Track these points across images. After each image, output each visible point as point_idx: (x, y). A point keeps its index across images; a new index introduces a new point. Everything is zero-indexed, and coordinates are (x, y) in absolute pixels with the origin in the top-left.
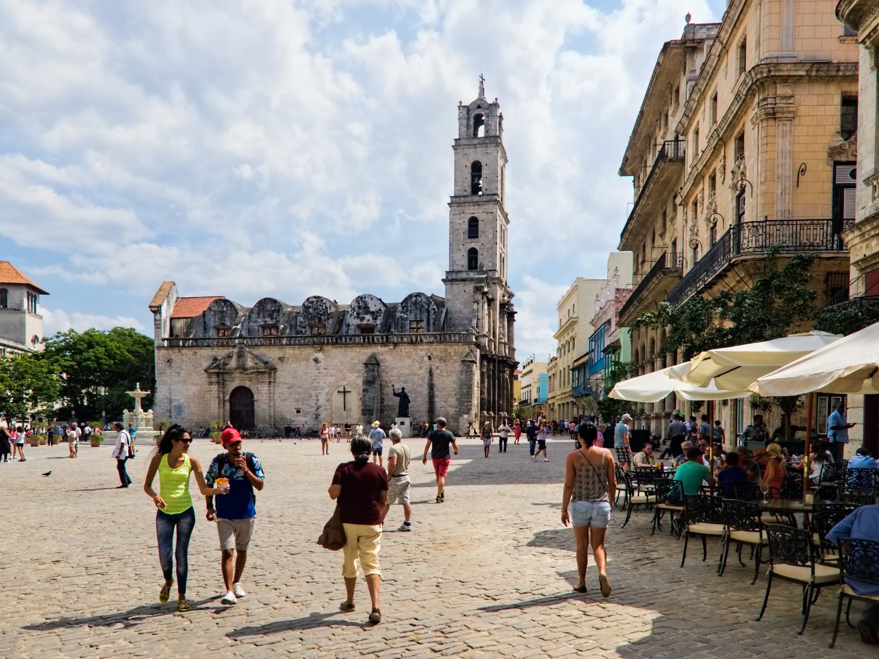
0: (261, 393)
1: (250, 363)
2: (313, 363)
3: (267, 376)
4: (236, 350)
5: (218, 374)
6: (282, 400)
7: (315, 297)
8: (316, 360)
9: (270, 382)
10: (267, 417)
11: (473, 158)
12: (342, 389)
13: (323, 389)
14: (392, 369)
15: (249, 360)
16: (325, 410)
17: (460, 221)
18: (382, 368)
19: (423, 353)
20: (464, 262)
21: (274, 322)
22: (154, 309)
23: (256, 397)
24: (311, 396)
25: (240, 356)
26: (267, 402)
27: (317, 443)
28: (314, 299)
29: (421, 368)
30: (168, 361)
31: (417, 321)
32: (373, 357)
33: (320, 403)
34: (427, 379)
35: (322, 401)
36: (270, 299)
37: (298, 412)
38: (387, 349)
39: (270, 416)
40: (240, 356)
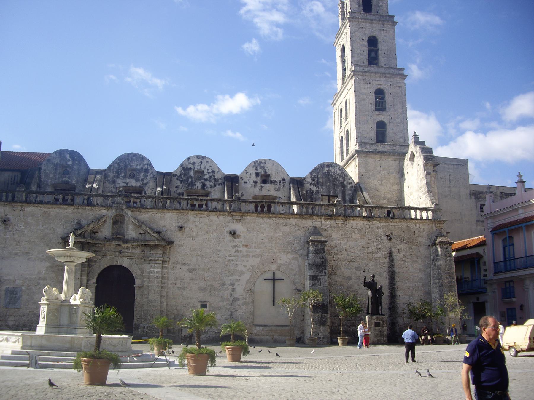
0: (148, 275)
1: (131, 232)
2: (229, 237)
3: (160, 252)
6: (179, 289)
7: (198, 157)
8: (233, 233)
9: (163, 262)
11: (369, 33)
12: (269, 276)
13: (242, 273)
14: (341, 251)
15: (131, 227)
16: (245, 304)
17: (366, 91)
19: (381, 231)
20: (372, 135)
21: (138, 184)
23: (138, 282)
24: (224, 284)
26: (159, 289)
28: (195, 160)
29: (379, 250)
31: (329, 196)
33: (236, 295)
34: (386, 265)
35: (240, 290)
38: (333, 222)
40: (118, 221)
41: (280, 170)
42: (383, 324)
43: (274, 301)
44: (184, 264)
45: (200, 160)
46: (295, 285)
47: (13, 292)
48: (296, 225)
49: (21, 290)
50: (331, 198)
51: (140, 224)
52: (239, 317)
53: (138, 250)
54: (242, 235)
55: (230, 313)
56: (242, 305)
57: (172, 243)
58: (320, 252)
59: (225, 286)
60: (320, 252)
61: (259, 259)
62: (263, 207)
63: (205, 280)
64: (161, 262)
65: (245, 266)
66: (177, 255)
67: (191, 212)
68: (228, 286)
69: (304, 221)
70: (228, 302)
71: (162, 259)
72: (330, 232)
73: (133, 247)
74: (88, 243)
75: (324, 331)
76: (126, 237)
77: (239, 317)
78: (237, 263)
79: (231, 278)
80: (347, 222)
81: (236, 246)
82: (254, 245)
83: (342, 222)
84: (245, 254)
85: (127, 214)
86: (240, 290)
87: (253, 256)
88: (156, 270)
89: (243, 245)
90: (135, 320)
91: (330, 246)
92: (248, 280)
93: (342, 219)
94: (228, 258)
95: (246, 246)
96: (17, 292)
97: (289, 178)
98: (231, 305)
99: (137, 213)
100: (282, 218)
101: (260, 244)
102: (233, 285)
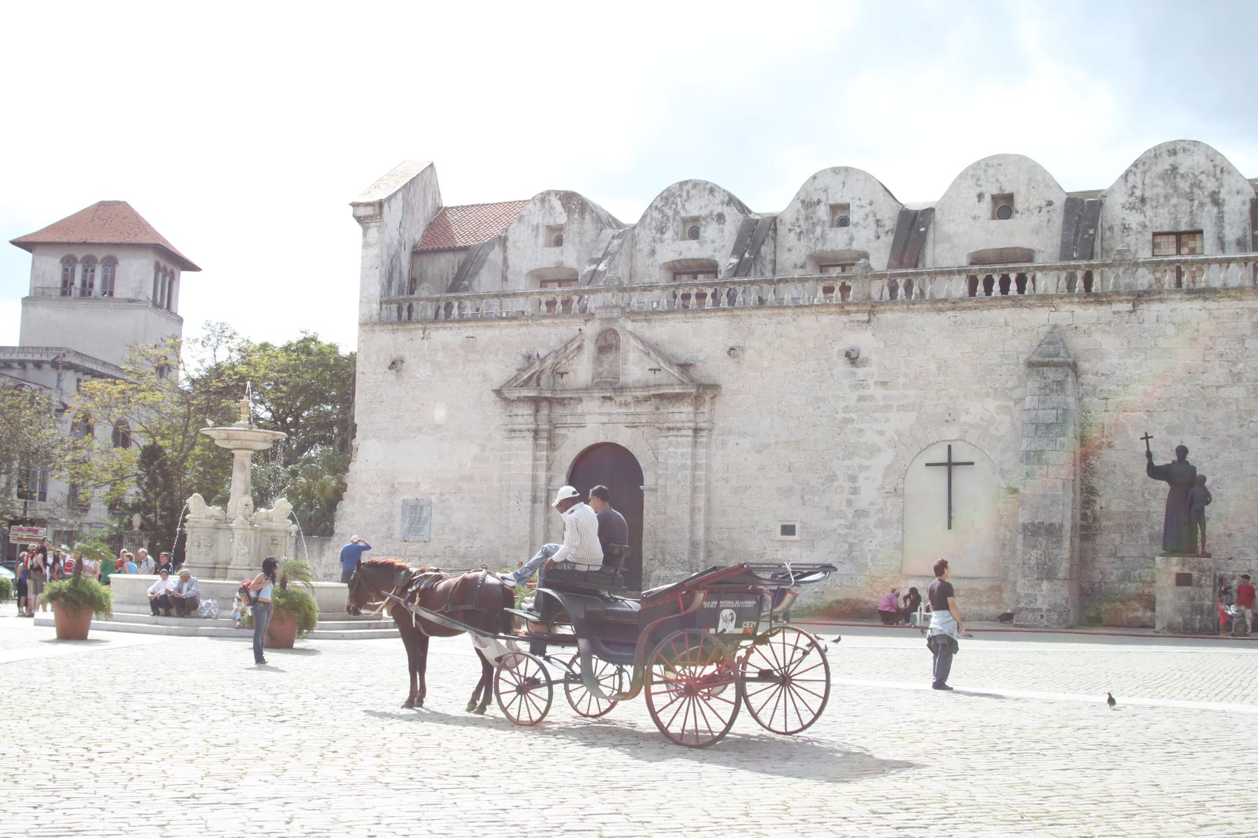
2: (842, 366)
4: (592, 329)
5: (536, 401)
7: (835, 171)
8: (852, 358)
10: (685, 547)
13: (873, 451)
16: (881, 524)
18: (1089, 379)
22: (362, 212)
24: (832, 478)
25: (607, 345)
27: (911, 651)
30: (393, 365)
32: (1055, 337)
33: (862, 502)
35: (869, 494)
36: (696, 184)
37: (788, 530)
39: (694, 544)
40: (607, 345)
41: (1040, 178)
42: (1200, 579)
43: (950, 517)
44: (744, 435)
45: (841, 176)
46: (1003, 477)
47: (415, 507)
48: (1006, 324)
49: (430, 504)
50: (1184, 239)
51: (651, 348)
52: (869, 556)
53: (647, 408)
54: (874, 358)
55: (846, 546)
56: (876, 527)
57: (715, 387)
58: (1052, 391)
59: (836, 483)
60: (1052, 391)
61: (915, 414)
62: (988, 283)
63: (790, 470)
64: (690, 432)
65: (881, 433)
66: (728, 413)
67: (755, 312)
68: (842, 482)
69: (1026, 313)
70: (842, 521)
71: (691, 425)
72: (1097, 337)
73: (638, 401)
74: (546, 399)
75: (1048, 595)
76: (622, 379)
77: (869, 556)
78: (863, 426)
79: (848, 462)
80: (1145, 306)
81: (861, 384)
82: (902, 380)
83: (1129, 306)
84: (881, 403)
85: (623, 328)
86: (869, 494)
87: (902, 408)
88: (679, 451)
89: (876, 383)
90: (644, 564)
91: (1096, 374)
92: (889, 467)
93: (1129, 301)
94: (841, 415)
95: (884, 384)
96: (422, 508)
97: (1064, 197)
98: (851, 526)
99: (645, 324)
100: (970, 308)
101: (916, 378)
102: (853, 478)
